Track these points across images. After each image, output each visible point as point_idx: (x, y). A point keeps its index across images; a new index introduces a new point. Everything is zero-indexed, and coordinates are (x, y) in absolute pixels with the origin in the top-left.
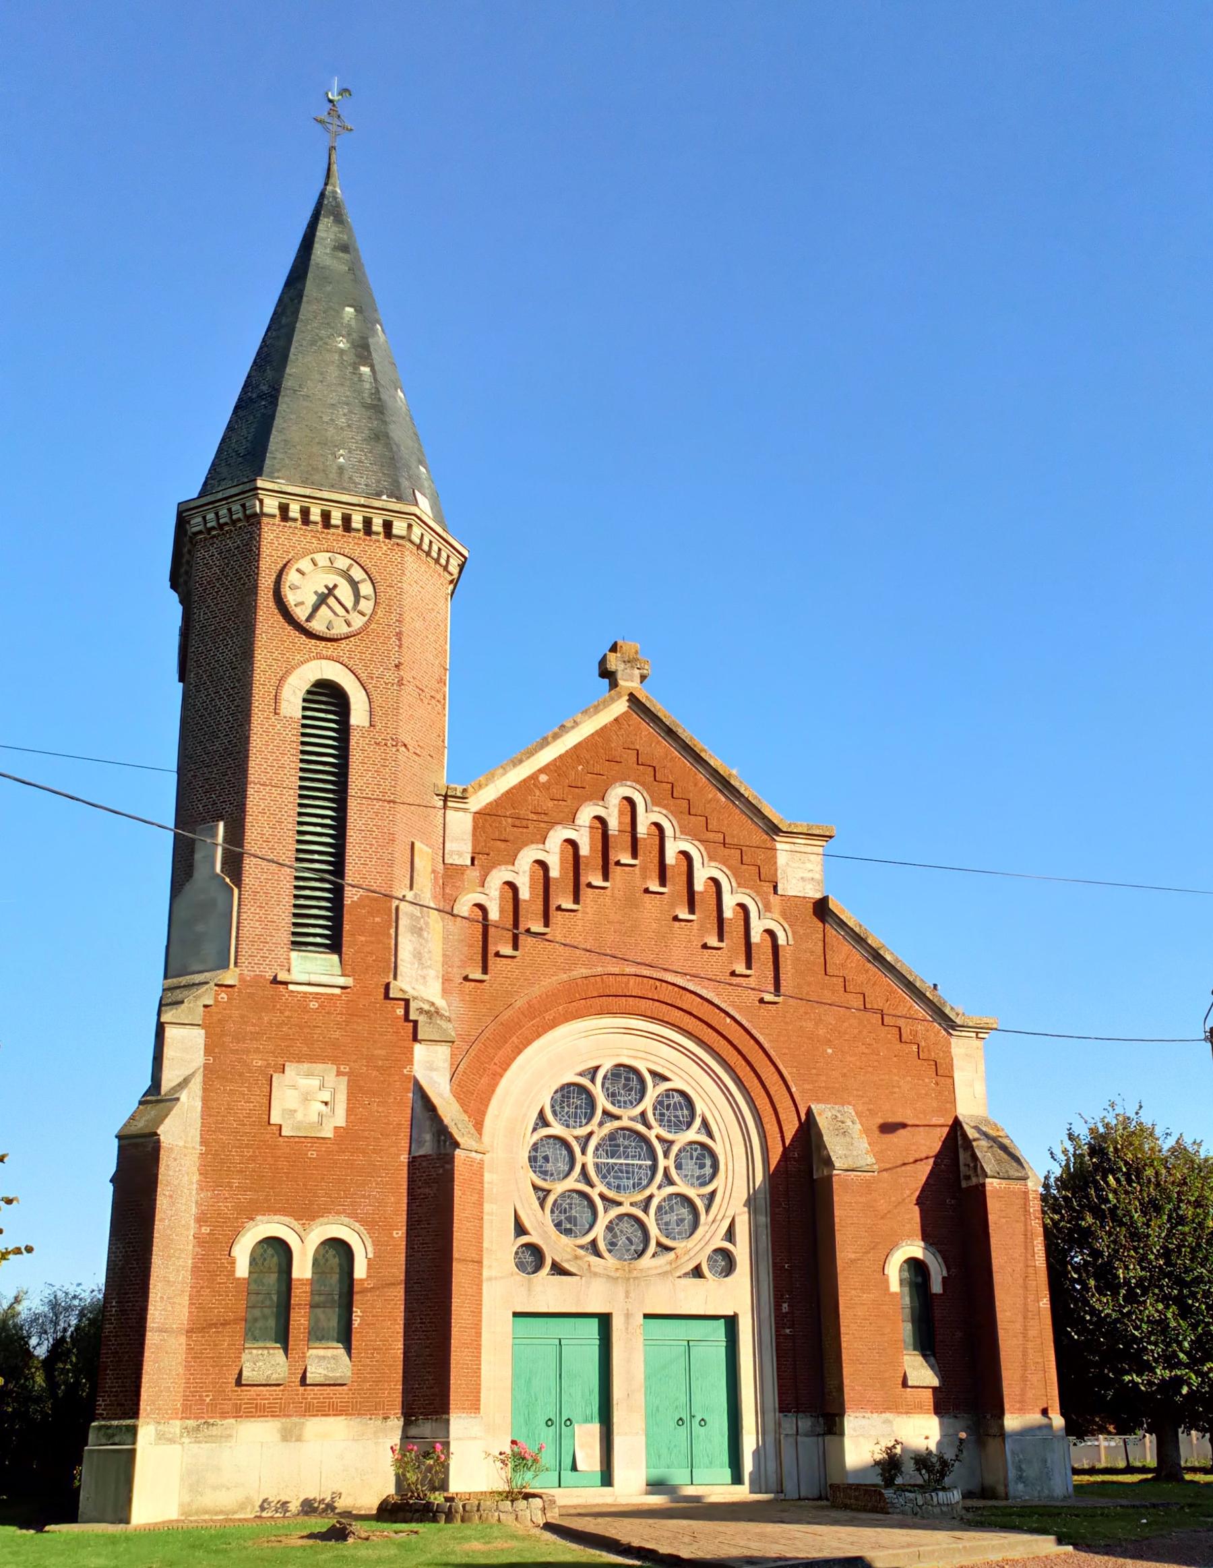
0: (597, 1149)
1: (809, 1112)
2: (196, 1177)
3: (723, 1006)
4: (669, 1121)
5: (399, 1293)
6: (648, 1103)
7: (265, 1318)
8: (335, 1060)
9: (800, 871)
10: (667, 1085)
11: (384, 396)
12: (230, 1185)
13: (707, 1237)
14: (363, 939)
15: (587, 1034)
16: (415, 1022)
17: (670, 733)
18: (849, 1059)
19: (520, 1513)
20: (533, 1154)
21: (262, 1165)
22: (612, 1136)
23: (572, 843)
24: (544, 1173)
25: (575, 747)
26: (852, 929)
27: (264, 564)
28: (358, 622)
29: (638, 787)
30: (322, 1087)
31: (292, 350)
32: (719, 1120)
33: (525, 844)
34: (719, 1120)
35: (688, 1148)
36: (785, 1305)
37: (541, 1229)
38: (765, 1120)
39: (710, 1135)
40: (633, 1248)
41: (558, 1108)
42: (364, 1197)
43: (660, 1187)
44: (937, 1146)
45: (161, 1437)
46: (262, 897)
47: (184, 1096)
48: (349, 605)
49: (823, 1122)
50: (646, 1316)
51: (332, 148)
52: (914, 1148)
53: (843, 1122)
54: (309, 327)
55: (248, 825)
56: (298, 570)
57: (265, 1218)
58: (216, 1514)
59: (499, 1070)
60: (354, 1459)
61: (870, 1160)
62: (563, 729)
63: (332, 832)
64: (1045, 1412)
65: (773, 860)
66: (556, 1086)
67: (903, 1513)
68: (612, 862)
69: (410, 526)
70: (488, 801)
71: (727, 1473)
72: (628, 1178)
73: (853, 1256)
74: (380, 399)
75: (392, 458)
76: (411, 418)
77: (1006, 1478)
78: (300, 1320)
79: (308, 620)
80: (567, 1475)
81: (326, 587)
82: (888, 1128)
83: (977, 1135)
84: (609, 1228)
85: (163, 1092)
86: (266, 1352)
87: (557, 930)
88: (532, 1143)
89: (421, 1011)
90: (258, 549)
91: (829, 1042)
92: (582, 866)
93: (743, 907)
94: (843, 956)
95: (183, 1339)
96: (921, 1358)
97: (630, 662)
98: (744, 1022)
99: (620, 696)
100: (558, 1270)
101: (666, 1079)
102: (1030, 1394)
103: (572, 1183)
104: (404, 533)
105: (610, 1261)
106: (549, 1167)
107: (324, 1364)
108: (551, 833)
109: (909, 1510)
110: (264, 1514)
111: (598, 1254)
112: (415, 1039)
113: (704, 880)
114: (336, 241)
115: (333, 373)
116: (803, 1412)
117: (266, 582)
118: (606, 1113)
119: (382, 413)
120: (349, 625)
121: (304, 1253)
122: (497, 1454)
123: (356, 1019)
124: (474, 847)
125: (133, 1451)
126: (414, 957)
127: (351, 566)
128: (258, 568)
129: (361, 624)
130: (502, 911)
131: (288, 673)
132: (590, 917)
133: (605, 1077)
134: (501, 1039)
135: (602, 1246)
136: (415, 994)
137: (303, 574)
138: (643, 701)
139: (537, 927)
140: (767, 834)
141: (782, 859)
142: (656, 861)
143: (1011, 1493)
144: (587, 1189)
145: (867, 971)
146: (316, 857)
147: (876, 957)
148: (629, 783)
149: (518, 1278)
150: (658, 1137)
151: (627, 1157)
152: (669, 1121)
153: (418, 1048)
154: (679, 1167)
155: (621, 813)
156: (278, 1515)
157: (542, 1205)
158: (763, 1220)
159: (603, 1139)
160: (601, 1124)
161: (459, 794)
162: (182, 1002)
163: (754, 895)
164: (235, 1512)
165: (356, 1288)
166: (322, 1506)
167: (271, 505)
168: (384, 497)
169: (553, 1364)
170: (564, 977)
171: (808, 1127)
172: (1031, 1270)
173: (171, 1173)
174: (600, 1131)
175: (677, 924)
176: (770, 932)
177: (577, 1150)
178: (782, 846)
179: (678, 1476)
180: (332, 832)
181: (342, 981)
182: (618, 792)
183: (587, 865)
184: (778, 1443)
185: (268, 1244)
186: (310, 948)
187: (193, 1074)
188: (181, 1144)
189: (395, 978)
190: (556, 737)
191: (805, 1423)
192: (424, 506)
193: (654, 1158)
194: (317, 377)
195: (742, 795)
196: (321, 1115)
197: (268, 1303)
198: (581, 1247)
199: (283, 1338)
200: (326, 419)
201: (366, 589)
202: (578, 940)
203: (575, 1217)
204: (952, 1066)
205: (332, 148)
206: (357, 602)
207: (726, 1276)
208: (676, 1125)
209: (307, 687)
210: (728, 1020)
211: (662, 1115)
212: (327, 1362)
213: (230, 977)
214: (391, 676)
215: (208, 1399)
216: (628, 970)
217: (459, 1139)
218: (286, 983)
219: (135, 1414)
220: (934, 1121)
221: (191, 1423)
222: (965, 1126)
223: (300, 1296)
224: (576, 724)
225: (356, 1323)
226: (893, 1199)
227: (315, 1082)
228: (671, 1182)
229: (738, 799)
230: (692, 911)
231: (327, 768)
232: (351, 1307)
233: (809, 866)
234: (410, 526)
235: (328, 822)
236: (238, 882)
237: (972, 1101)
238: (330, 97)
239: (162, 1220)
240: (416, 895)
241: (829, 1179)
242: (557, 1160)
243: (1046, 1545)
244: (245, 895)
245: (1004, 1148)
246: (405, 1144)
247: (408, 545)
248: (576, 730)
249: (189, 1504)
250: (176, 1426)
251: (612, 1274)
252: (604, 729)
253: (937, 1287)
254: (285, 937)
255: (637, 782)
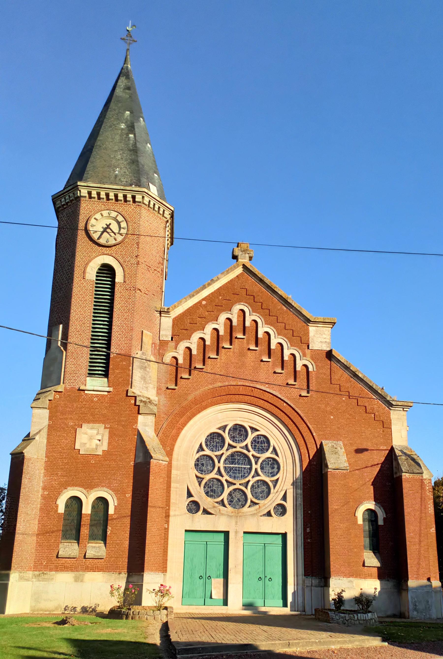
0: (225, 460)
1: (321, 444)
2: (43, 471)
3: (282, 398)
4: (258, 448)
5: (128, 521)
6: (248, 441)
7: (71, 530)
8: (103, 422)
9: (320, 338)
10: (258, 433)
11: (138, 145)
12: (57, 474)
13: (274, 499)
14: (118, 371)
15: (221, 411)
16: (139, 406)
17: (261, 281)
18: (341, 420)
19: (156, 616)
20: (197, 462)
21: (68, 465)
22: (232, 455)
23: (216, 330)
24: (201, 471)
25: (218, 289)
26: (343, 363)
27: (81, 217)
28: (120, 238)
29: (246, 305)
30: (98, 434)
31: (101, 130)
32: (281, 448)
33: (195, 331)
34: (281, 448)
35: (267, 460)
36: (308, 529)
37: (199, 494)
38: (301, 448)
39: (277, 454)
40: (240, 503)
41: (208, 443)
42: (114, 479)
43: (253, 477)
44: (383, 459)
45: (21, 578)
46: (75, 355)
47: (37, 438)
48: (116, 231)
49: (326, 448)
50: (245, 533)
51: (128, 50)
52: (371, 460)
53: (336, 448)
54: (109, 121)
55: (70, 325)
56: (95, 219)
57: (71, 488)
58: (46, 611)
59: (181, 427)
60: (101, 589)
61: (346, 464)
62: (213, 281)
63: (107, 327)
64: (429, 579)
65: (307, 333)
66: (208, 433)
67: (338, 623)
68: (234, 337)
69: (143, 197)
70: (179, 313)
71: (281, 602)
72: (239, 473)
73: (337, 507)
74: (136, 147)
75: (139, 170)
76: (153, 155)
77: (408, 608)
78: (85, 531)
79: (98, 239)
80: (208, 600)
81: (106, 225)
82: (359, 451)
83: (401, 454)
84: (230, 494)
85: (30, 436)
86: (70, 544)
87: (209, 367)
88: (196, 458)
89: (141, 401)
90: (79, 211)
91: (331, 413)
92: (220, 339)
93: (293, 355)
94: (339, 375)
95: (35, 538)
96: (372, 554)
97: (245, 251)
98: (292, 405)
99: (238, 266)
100: (206, 512)
101: (257, 430)
102: (421, 571)
103: (213, 475)
104: (141, 200)
105: (230, 509)
106: (204, 468)
107: (94, 550)
108: (207, 326)
109: (341, 622)
110: (66, 612)
111: (224, 505)
112: (139, 413)
113: (275, 344)
114: (125, 86)
115: (117, 138)
116: (315, 576)
117: (81, 225)
118: (229, 445)
119: (136, 152)
120: (115, 240)
121: (87, 503)
122: (152, 590)
123: (114, 405)
124: (173, 333)
125: (142, 585)
126: (142, 379)
127: (118, 215)
128: (78, 219)
129: (121, 239)
130: (184, 359)
131: (90, 261)
132: (223, 361)
133: (230, 430)
134: (181, 414)
135: (226, 502)
136: (140, 394)
137: (97, 220)
138: (249, 267)
139: (200, 366)
140: (305, 323)
141: (311, 334)
142: (254, 336)
143: (410, 616)
144: (220, 478)
145: (350, 382)
146: (100, 338)
147: (355, 375)
148: (242, 303)
149: (188, 515)
150: (253, 455)
151: (239, 464)
152: (258, 448)
153: (140, 417)
154: (262, 468)
155: (239, 316)
156: (72, 613)
157: (200, 485)
158: (299, 491)
159: (228, 456)
160: (227, 450)
161: (166, 310)
162: (39, 399)
163: (298, 350)
164: (53, 611)
165: (109, 518)
166: (91, 610)
167: (84, 192)
168: (133, 186)
169: (203, 553)
170: (211, 387)
171: (320, 451)
172: (423, 515)
173: (30, 469)
174: (226, 453)
175: (262, 363)
176: (306, 366)
177: (216, 461)
178: (312, 329)
179: (259, 603)
180: (107, 327)
181: (108, 389)
182: (237, 308)
183: (222, 339)
184: (303, 590)
185: (74, 500)
186: (96, 376)
187: (42, 429)
188: (35, 457)
189: (131, 388)
190: (209, 285)
191: (315, 581)
192: (153, 190)
193: (250, 464)
194: (110, 140)
195: (293, 306)
196: (97, 445)
197: (72, 524)
198: (217, 502)
199: (78, 539)
200: (112, 156)
201: (123, 225)
202: (218, 371)
203: (215, 490)
204: (391, 423)
205: (128, 50)
206: (120, 230)
207: (282, 516)
208: (261, 450)
209: (99, 267)
210: (285, 404)
211: (255, 446)
212: (96, 549)
213: (60, 388)
214: (133, 261)
215: (44, 563)
216: (239, 383)
217: (153, 455)
218: (84, 390)
219: (144, 572)
220: (381, 448)
221: (37, 573)
222: (396, 450)
223: (85, 521)
224: (218, 279)
225: (109, 533)
226: (361, 482)
227: (95, 432)
228: (258, 475)
229: (292, 308)
230: (270, 357)
231: (106, 301)
232: (107, 526)
233: (324, 336)
234: (143, 197)
235: (106, 323)
236: (66, 349)
237: (400, 438)
238: (128, 29)
239: (24, 488)
240: (143, 353)
241: (327, 473)
242: (207, 465)
243: (375, 642)
244: (68, 354)
245: (413, 460)
246: (133, 457)
247: (143, 205)
248: (219, 281)
249: (34, 607)
250: (30, 574)
251: (230, 514)
252: (231, 282)
253: (381, 522)
254: (85, 370)
255: (246, 303)
